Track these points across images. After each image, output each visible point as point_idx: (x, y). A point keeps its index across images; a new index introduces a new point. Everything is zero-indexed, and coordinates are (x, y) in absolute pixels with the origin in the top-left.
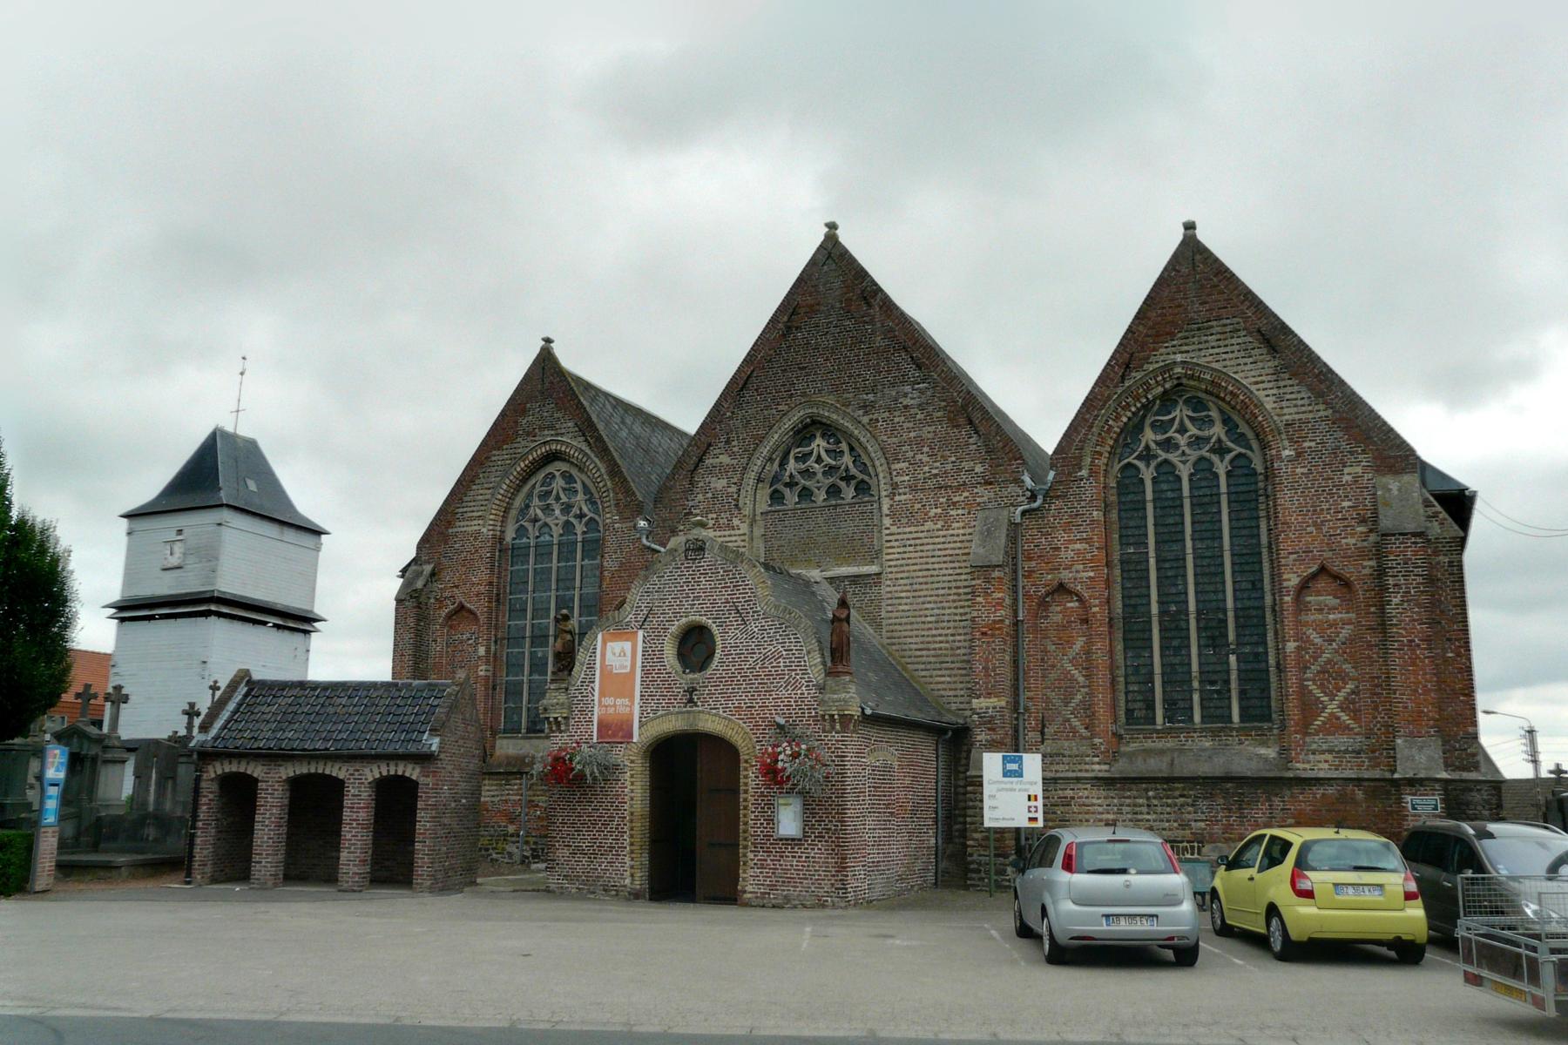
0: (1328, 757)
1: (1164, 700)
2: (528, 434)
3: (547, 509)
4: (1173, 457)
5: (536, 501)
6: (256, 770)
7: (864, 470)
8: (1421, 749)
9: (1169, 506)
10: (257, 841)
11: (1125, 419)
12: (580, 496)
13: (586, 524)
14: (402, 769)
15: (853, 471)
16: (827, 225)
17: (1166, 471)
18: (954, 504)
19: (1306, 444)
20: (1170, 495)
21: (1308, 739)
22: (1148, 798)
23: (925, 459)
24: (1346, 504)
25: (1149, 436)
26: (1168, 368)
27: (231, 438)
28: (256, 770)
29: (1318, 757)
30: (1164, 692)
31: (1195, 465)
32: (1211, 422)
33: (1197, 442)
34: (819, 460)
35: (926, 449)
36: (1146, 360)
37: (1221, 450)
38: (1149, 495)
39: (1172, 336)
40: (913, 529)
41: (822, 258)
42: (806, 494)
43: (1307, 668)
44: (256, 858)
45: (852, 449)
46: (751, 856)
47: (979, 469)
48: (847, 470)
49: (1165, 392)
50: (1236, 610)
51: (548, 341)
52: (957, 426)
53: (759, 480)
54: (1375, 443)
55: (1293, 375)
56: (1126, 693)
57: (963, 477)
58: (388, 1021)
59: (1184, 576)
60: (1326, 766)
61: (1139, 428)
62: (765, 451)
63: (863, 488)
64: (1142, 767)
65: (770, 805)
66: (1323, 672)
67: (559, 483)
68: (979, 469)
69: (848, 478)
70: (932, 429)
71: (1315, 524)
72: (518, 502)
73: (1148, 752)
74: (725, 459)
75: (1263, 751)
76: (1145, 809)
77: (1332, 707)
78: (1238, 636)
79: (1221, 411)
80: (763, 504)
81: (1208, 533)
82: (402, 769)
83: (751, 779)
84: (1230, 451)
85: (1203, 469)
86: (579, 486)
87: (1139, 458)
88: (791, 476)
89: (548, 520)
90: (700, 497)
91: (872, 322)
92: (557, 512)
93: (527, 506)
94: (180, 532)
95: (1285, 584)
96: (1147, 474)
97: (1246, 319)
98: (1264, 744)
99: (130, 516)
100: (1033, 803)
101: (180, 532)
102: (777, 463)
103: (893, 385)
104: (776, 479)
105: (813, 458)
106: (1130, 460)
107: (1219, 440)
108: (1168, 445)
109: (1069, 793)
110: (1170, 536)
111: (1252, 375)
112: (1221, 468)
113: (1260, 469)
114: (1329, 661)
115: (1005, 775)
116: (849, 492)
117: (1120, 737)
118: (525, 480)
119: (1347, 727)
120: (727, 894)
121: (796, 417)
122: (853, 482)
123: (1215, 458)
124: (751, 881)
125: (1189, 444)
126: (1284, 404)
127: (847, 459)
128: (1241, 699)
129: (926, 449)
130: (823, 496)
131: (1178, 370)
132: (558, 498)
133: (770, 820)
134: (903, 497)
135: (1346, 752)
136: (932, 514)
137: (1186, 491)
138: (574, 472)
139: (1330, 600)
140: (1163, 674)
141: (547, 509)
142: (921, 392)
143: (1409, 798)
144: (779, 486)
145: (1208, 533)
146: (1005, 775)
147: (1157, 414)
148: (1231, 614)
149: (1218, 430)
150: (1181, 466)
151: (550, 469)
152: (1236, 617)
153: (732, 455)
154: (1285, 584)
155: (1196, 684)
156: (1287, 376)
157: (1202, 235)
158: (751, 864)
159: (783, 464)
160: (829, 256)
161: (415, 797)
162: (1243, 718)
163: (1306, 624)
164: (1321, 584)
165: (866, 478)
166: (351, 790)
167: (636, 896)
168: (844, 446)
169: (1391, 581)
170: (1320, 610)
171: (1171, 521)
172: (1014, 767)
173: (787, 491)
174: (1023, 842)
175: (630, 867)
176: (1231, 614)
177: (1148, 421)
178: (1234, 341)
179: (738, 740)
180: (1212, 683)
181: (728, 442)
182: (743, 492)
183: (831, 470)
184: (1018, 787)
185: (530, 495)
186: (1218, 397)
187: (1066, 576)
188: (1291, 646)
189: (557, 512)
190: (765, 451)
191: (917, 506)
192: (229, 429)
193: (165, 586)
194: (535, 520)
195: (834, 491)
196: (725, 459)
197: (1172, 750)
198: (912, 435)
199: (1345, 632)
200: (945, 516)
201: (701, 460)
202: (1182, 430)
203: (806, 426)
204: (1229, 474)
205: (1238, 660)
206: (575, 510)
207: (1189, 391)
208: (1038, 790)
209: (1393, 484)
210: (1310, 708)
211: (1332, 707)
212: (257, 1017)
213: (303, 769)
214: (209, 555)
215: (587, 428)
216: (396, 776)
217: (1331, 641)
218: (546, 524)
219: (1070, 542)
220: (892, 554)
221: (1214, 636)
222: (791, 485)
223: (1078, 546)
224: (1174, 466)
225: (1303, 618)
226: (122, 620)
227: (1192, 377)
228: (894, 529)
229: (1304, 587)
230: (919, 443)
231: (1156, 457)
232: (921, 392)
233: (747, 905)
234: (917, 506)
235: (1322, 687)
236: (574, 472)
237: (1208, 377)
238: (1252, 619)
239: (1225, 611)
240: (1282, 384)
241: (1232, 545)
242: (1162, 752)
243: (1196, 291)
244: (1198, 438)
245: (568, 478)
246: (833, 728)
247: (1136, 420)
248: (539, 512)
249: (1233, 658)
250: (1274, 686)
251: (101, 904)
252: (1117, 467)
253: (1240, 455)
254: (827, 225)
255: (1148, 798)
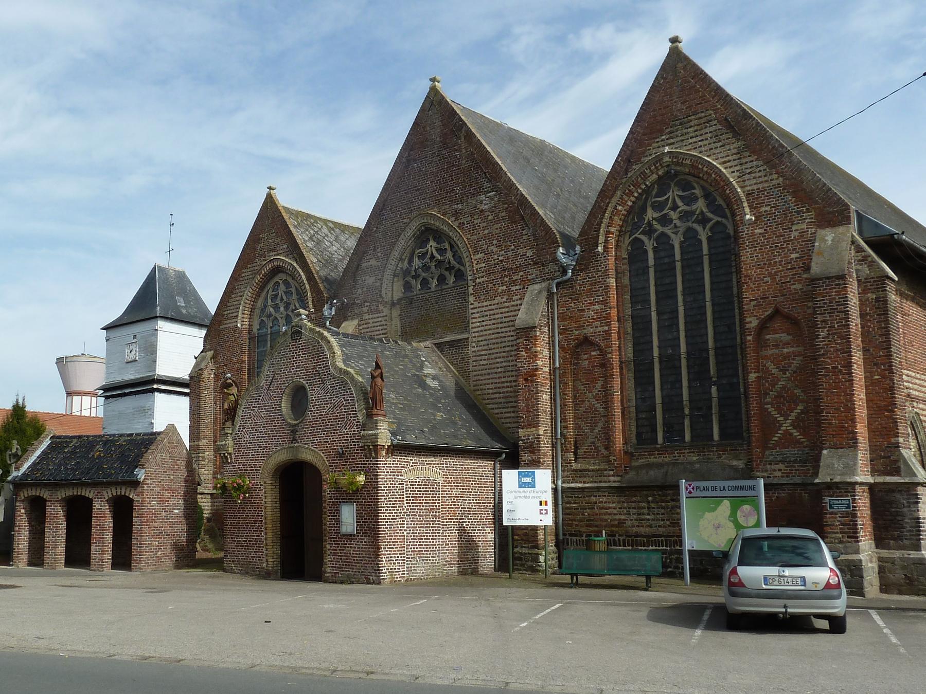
0: (781, 466)
1: (664, 424)
2: (261, 256)
3: (276, 307)
4: (668, 231)
5: (269, 301)
6: (45, 494)
7: (461, 262)
8: (840, 457)
9: (665, 270)
10: (47, 539)
11: (630, 203)
12: (294, 296)
13: (657, 240)
14: (123, 491)
15: (453, 262)
16: (431, 80)
17: (663, 242)
18: (514, 281)
19: (763, 209)
20: (666, 260)
21: (767, 453)
22: (648, 502)
23: (495, 249)
24: (793, 256)
25: (650, 214)
26: (659, 159)
27: (161, 269)
28: (45, 494)
29: (773, 467)
30: (664, 418)
31: (685, 234)
32: (696, 199)
33: (685, 216)
34: (432, 257)
35: (495, 242)
36: (643, 154)
37: (703, 221)
38: (651, 262)
39: (661, 132)
40: (488, 303)
41: (428, 105)
42: (425, 283)
43: (766, 394)
44: (46, 550)
45: (452, 246)
46: (328, 547)
47: (529, 253)
48: (449, 263)
49: (660, 177)
50: (716, 349)
51: (270, 188)
52: (515, 222)
53: (394, 276)
54: (816, 203)
55: (754, 152)
56: (637, 420)
57: (520, 261)
58: (130, 658)
59: (678, 325)
60: (779, 474)
61: (643, 210)
62: (396, 254)
63: (460, 275)
64: (646, 477)
65: (338, 511)
66: (779, 396)
67: (282, 288)
68: (529, 253)
69: (450, 269)
70: (498, 226)
71: (770, 275)
72: (260, 304)
73: (650, 466)
74: (373, 262)
75: (735, 463)
76: (646, 511)
77: (786, 426)
78: (718, 370)
79: (703, 188)
80: (398, 291)
81: (694, 289)
82: (123, 491)
83: (327, 491)
84: (711, 220)
85: (691, 237)
86: (293, 290)
87: (643, 233)
88: (416, 270)
89: (278, 316)
90: (360, 291)
91: (459, 150)
92: (282, 309)
93: (265, 306)
94: (135, 337)
95: (747, 326)
96: (649, 245)
97: (716, 111)
98: (737, 458)
99: (106, 328)
100: (543, 507)
101: (135, 337)
102: (406, 263)
103: (474, 195)
104: (406, 273)
105: (428, 256)
106: (636, 235)
107: (702, 212)
108: (665, 220)
109: (593, 499)
110: (666, 294)
111: (722, 161)
112: (703, 236)
113: (732, 233)
114: (784, 387)
115: (520, 486)
116: (451, 279)
117: (632, 455)
118: (262, 289)
119: (798, 442)
120: (317, 576)
121: (414, 227)
122: (453, 272)
123: (699, 228)
124: (329, 565)
125: (680, 218)
126: (746, 177)
127: (449, 255)
128: (720, 422)
129: (495, 242)
130: (435, 282)
131: (667, 159)
132: (282, 299)
133: (338, 522)
134: (481, 280)
135: (795, 461)
136: (500, 291)
137: (678, 256)
138: (290, 280)
139: (784, 337)
140: (663, 403)
141: (276, 307)
142: (492, 199)
143: (827, 499)
144: (409, 279)
145: (694, 289)
146: (520, 486)
147: (657, 196)
148: (711, 353)
149: (700, 205)
150: (673, 236)
151: (276, 279)
152: (716, 355)
153: (377, 259)
154: (747, 326)
155: (687, 411)
156: (748, 154)
157: (683, 47)
158: (328, 552)
159: (411, 261)
160: (432, 103)
161: (131, 510)
162: (722, 435)
163: (765, 358)
164: (777, 324)
165: (462, 268)
166: (97, 505)
167: (266, 575)
168: (447, 245)
169: (820, 318)
170: (777, 346)
171: (667, 281)
172: (528, 480)
173: (413, 282)
174: (561, 537)
175: (269, 557)
176: (711, 353)
177: (649, 204)
178: (707, 130)
179: (319, 465)
180: (699, 409)
181: (374, 250)
182: (384, 285)
183: (440, 263)
184: (531, 495)
185: (266, 299)
186: (699, 177)
187: (589, 331)
188: (752, 376)
189: (282, 309)
190: (396, 254)
191: (491, 285)
192: (164, 264)
193: (130, 375)
194: (270, 316)
195: (442, 279)
196: (373, 262)
197: (668, 464)
198: (486, 232)
199: (796, 362)
200: (508, 292)
201: (359, 265)
202: (675, 208)
203: (422, 233)
204: (709, 239)
205: (718, 390)
206: (292, 307)
207: (687, 177)
208: (549, 497)
209: (828, 236)
210: (768, 426)
211: (786, 426)
212: (78, 655)
213: (70, 492)
214: (150, 350)
215: (295, 250)
216: (77, 496)
217: (784, 370)
218: (276, 318)
219: (591, 304)
220: (475, 323)
221: (699, 374)
222: (416, 277)
223: (597, 307)
224: (669, 237)
225: (764, 353)
226: (107, 398)
227: (677, 164)
228: (476, 305)
229: (763, 327)
230: (489, 238)
231: (656, 230)
232: (492, 199)
233: (327, 581)
234: (491, 285)
235: (779, 409)
236: (290, 280)
237: (688, 162)
238: (730, 354)
239: (707, 350)
240: (744, 161)
241: (712, 296)
242: (660, 466)
243: (681, 92)
244: (686, 212)
245: (286, 283)
246: (371, 454)
247: (640, 203)
248: (272, 310)
249: (714, 389)
250: (743, 409)
251: (502, 590)
252: (627, 241)
253: (718, 223)
254: (431, 80)
255: (648, 502)
